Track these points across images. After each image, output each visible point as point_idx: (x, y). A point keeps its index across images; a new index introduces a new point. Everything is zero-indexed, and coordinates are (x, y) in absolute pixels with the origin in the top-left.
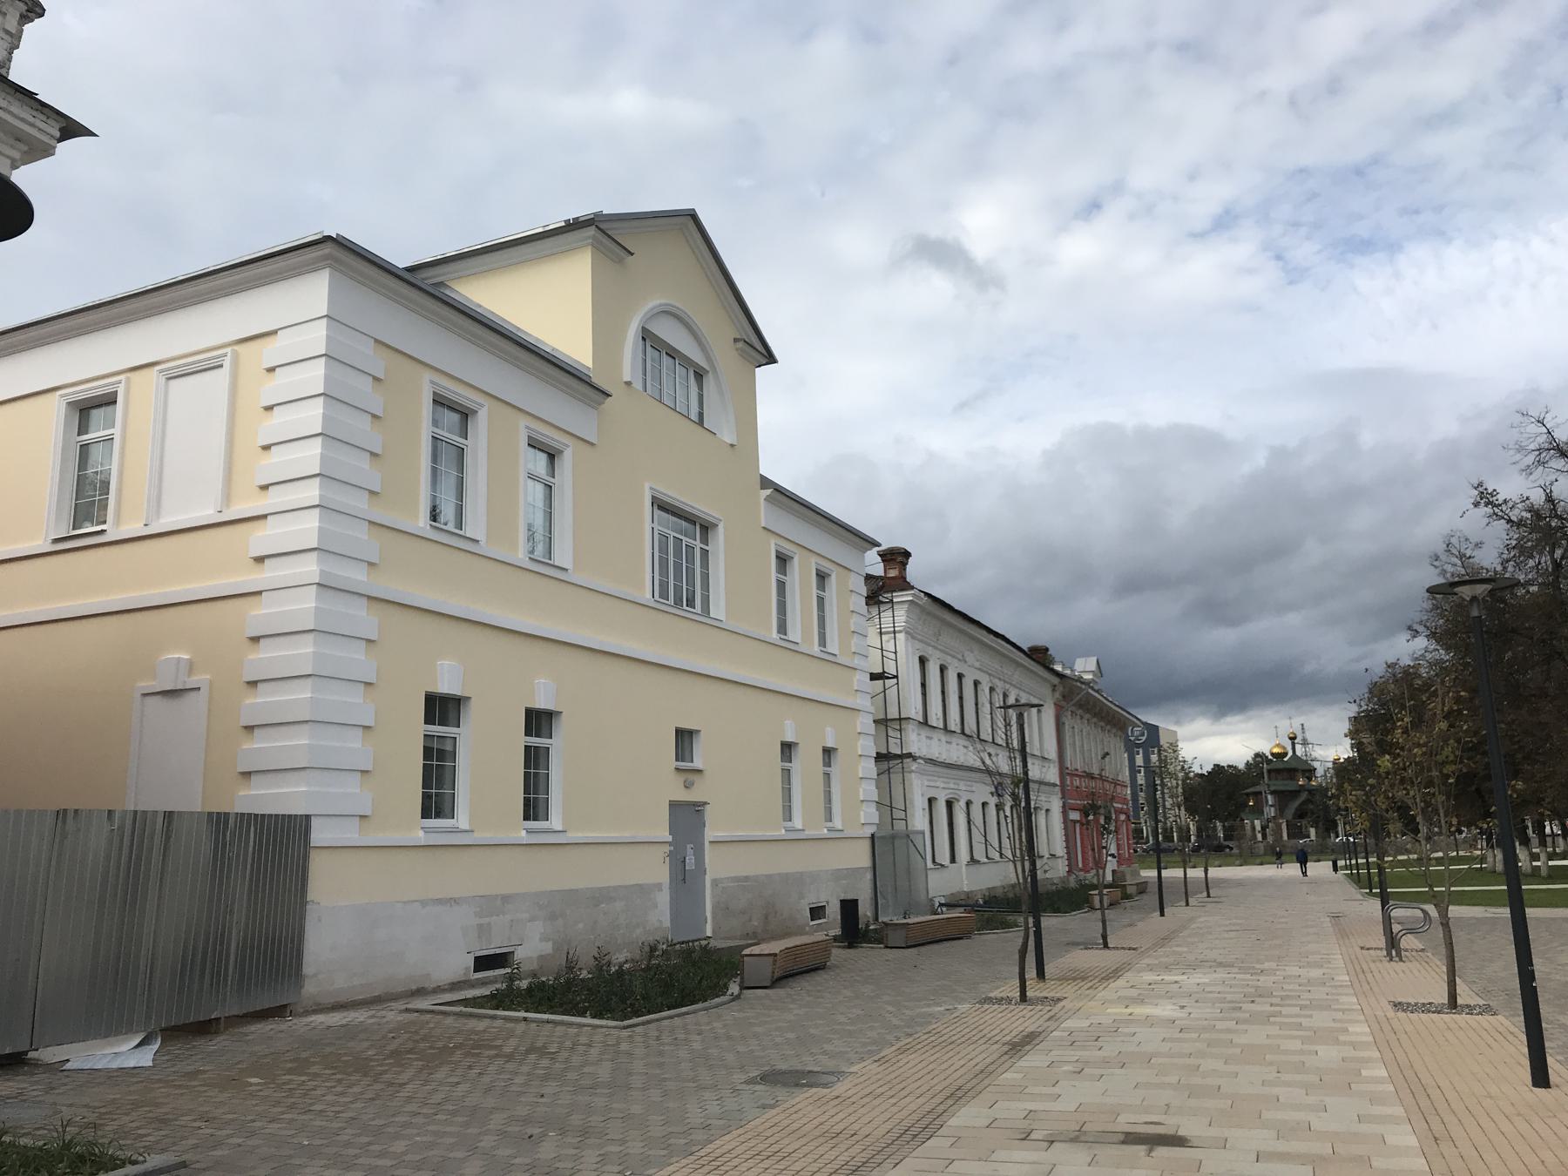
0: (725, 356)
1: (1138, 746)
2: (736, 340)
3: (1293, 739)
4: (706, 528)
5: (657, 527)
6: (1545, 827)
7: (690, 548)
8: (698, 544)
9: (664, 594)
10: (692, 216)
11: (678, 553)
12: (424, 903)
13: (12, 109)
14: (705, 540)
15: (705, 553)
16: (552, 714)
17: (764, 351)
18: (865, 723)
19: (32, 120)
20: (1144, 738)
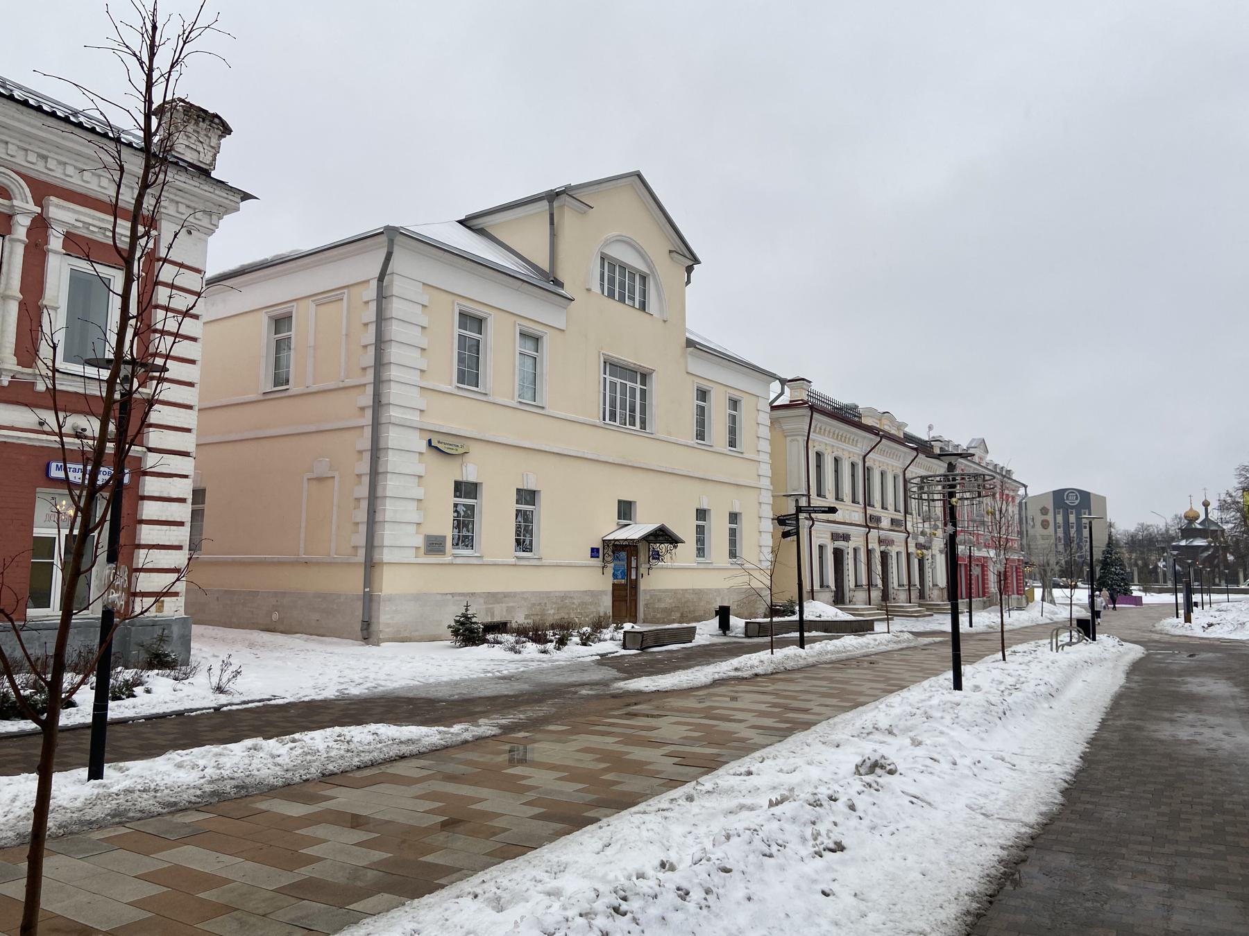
0: (666, 270)
1: (1072, 507)
2: (670, 252)
3: (1206, 504)
4: (645, 377)
5: (607, 376)
6: (124, 474)
7: (633, 390)
8: (638, 386)
9: (613, 416)
10: (639, 175)
11: (623, 393)
12: (453, 595)
13: (217, 192)
14: (644, 383)
15: (643, 392)
16: (476, 484)
17: (692, 258)
18: (767, 497)
19: (225, 195)
20: (1077, 502)
